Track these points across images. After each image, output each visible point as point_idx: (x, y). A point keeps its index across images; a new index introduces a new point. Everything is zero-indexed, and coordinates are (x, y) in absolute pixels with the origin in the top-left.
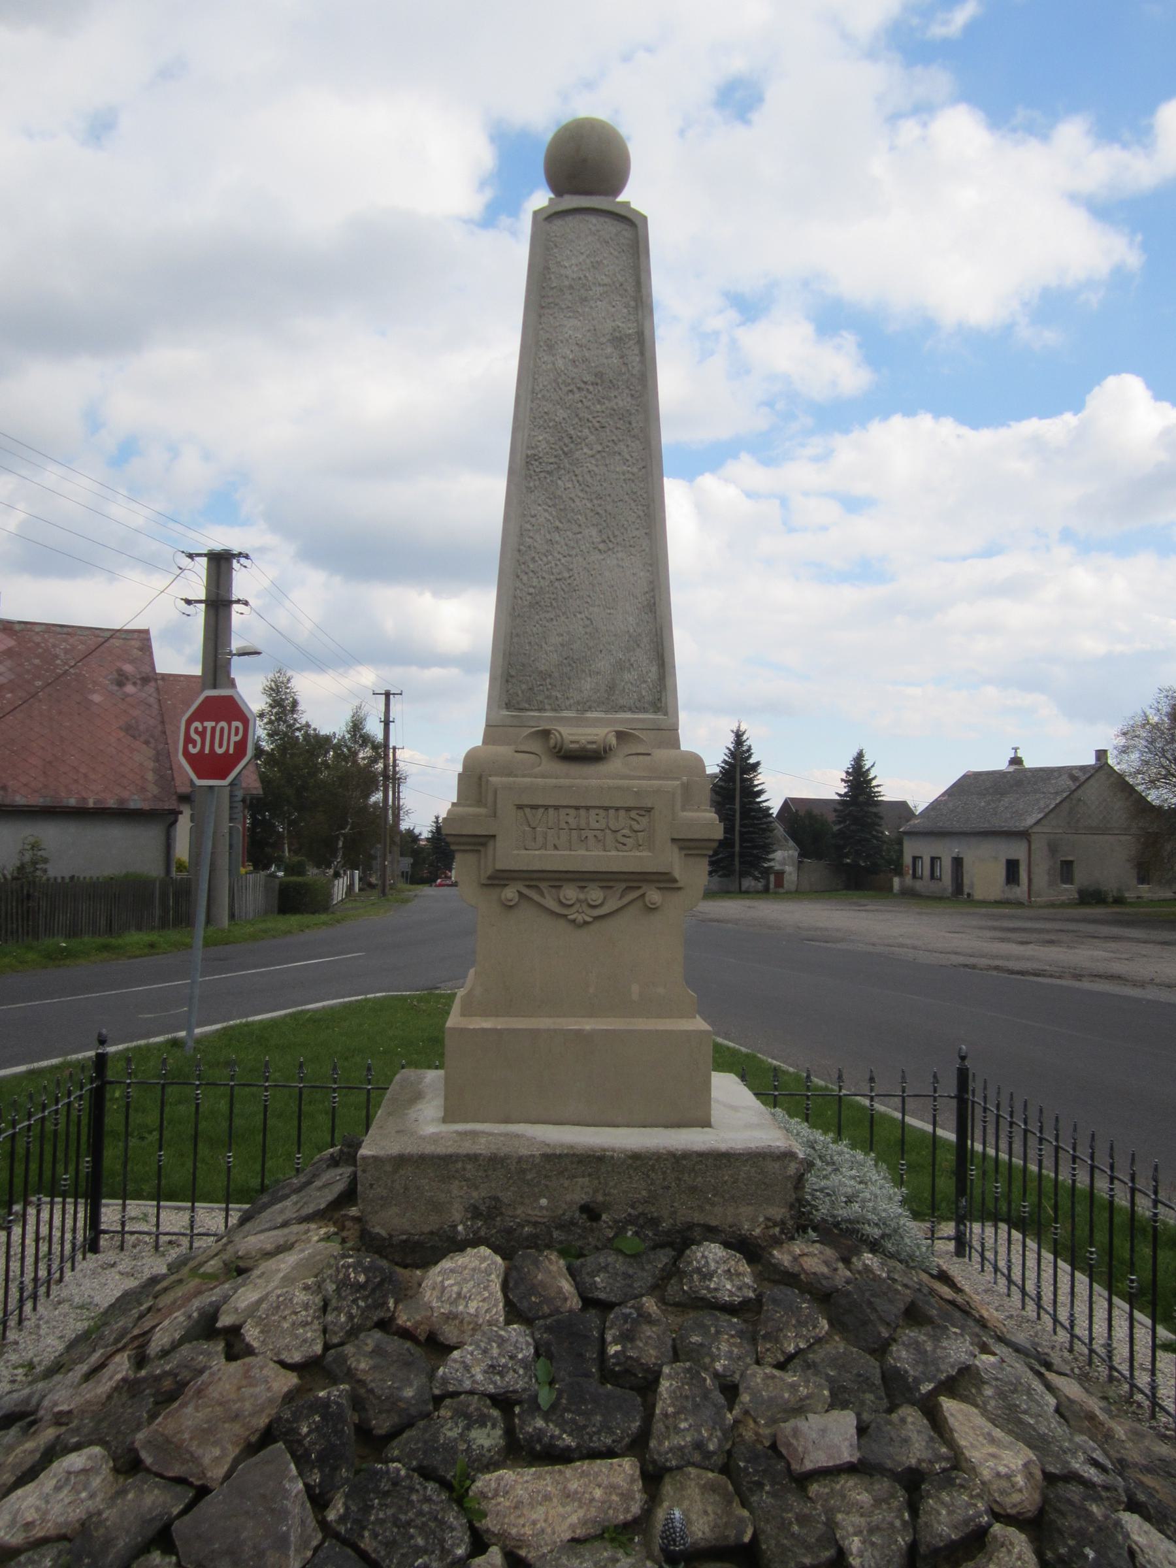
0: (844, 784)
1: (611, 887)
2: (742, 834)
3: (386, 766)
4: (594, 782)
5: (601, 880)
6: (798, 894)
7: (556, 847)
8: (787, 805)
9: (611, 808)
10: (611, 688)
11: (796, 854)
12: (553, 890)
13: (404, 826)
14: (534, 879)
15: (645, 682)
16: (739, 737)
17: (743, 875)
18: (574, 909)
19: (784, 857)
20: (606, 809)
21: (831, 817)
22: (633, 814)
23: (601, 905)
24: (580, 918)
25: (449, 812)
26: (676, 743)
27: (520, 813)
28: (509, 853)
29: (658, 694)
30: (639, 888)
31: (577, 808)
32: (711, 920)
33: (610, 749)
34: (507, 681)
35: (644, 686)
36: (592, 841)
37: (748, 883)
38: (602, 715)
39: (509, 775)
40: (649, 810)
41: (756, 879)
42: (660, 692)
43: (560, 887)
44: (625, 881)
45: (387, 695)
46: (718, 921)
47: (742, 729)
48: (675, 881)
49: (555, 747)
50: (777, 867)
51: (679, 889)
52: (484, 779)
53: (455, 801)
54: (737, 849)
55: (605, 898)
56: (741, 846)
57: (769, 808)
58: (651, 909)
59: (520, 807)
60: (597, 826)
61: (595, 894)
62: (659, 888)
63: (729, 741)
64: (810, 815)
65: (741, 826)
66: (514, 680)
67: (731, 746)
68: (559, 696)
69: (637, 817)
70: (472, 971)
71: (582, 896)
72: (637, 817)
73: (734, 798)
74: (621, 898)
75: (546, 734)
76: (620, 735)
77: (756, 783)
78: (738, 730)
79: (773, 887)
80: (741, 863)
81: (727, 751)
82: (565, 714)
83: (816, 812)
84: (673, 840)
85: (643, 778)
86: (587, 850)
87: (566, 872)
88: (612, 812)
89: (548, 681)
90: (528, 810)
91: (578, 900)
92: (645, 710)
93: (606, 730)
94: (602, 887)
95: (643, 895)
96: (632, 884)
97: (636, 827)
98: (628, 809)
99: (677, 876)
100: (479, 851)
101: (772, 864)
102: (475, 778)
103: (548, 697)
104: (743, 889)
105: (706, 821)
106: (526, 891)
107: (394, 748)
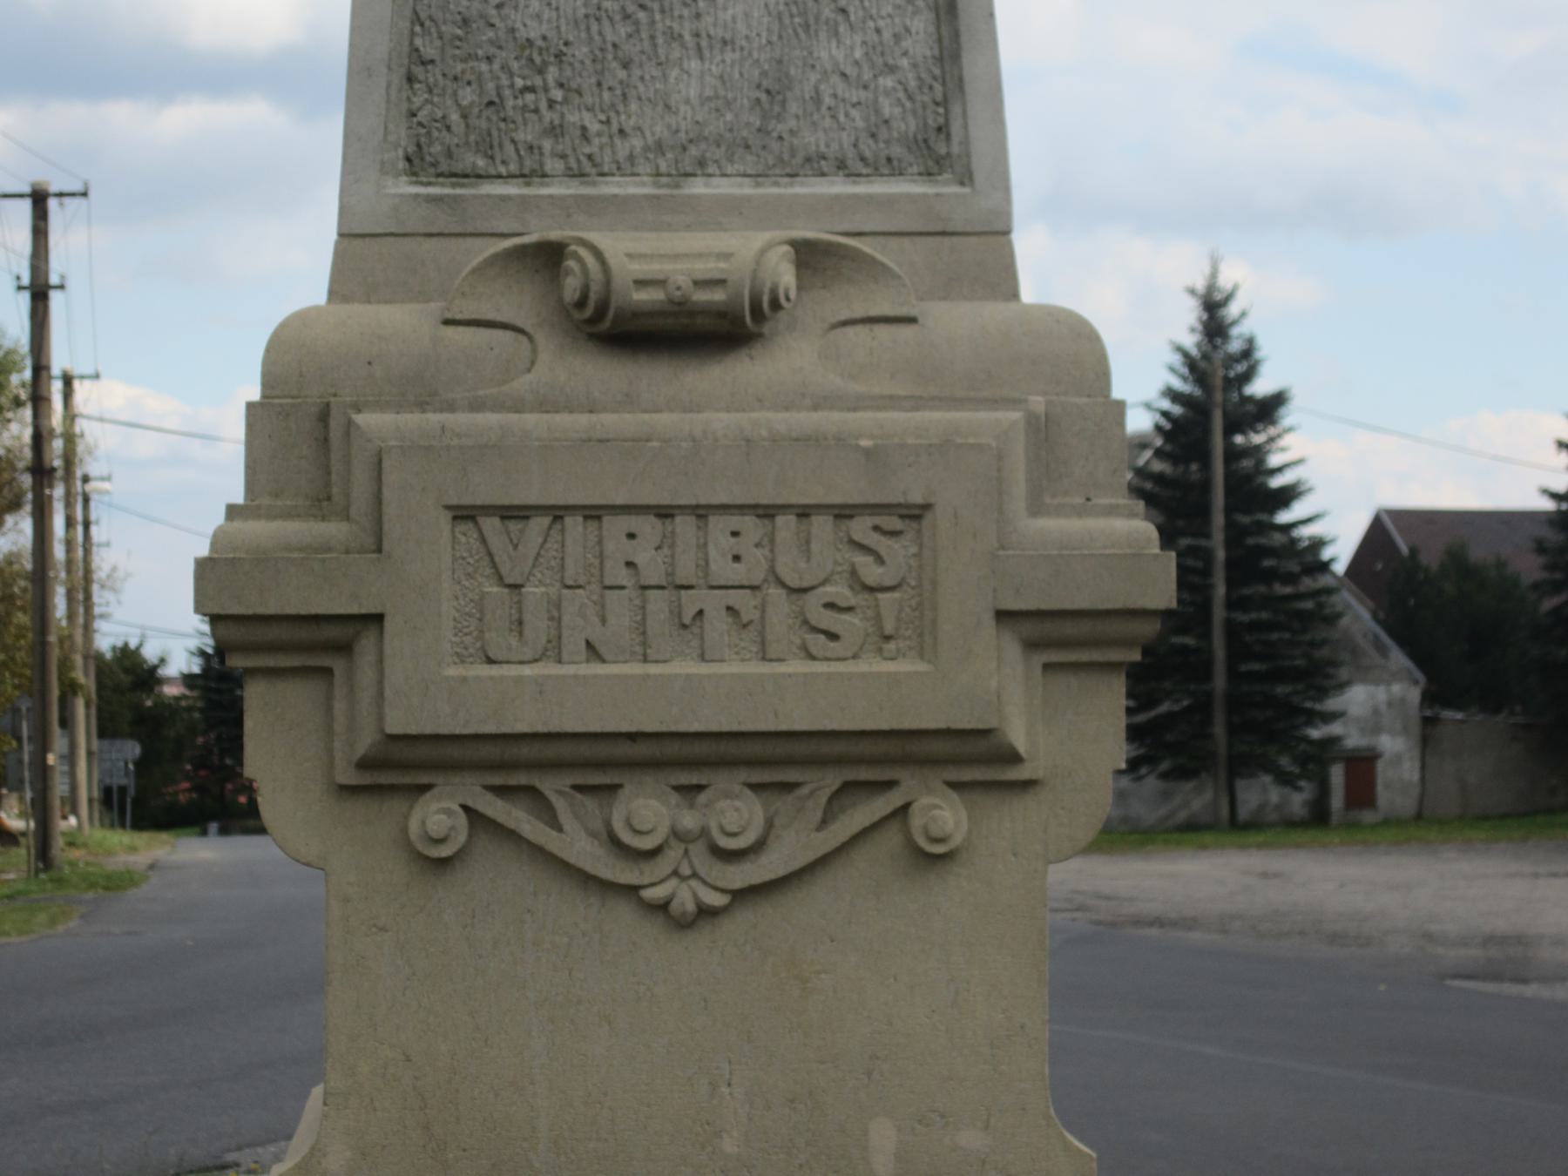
0: (1541, 560)
1: (789, 787)
2: (1232, 629)
3: (39, 440)
4: (721, 421)
5: (750, 763)
6: (1426, 822)
7: (593, 651)
8: (1380, 535)
9: (784, 508)
10: (773, 94)
11: (1414, 695)
12: (589, 803)
13: (109, 655)
14: (517, 763)
15: (892, 69)
16: (1214, 314)
17: (1239, 766)
18: (664, 865)
19: (1373, 706)
20: (767, 512)
21: (1529, 568)
22: (860, 528)
23: (758, 847)
24: (685, 898)
25: (217, 540)
26: (1002, 281)
27: (467, 534)
28: (432, 679)
29: (940, 114)
30: (890, 785)
31: (664, 513)
32: (1138, 922)
33: (776, 305)
34: (410, 79)
35: (888, 82)
36: (717, 624)
37: (1257, 793)
38: (747, 189)
39: (422, 406)
40: (915, 513)
41: (1285, 780)
42: (945, 102)
43: (614, 788)
44: (839, 761)
45: (39, 199)
46: (1159, 922)
47: (1225, 281)
48: (1014, 758)
49: (581, 304)
50: (1354, 741)
51: (1028, 785)
52: (336, 424)
53: (239, 498)
54: (1220, 682)
55: (769, 825)
56: (1232, 673)
57: (1318, 544)
58: (931, 860)
59: (464, 515)
60: (736, 573)
61: (735, 811)
62: (955, 786)
63: (1184, 326)
64: (1457, 561)
65: (1231, 605)
66: (434, 75)
67: (1190, 341)
68: (594, 127)
69: (873, 540)
70: (317, 1092)
71: (689, 821)
72: (873, 540)
73: (1204, 511)
74: (824, 823)
75: (550, 256)
76: (809, 256)
77: (1274, 460)
78: (1211, 287)
79: (1340, 799)
80: (1232, 730)
81: (1177, 360)
82: (611, 187)
83: (1478, 553)
84: (1003, 616)
85: (892, 402)
86: (703, 658)
87: (633, 737)
88: (786, 522)
89: (552, 73)
90: (490, 525)
91: (676, 834)
92: (893, 168)
93: (760, 239)
94: (756, 788)
95: (904, 809)
96: (865, 774)
97: (872, 573)
98: (843, 513)
99: (1021, 743)
100: (328, 672)
101: (1335, 729)
102: (305, 424)
103: (555, 131)
104: (1243, 813)
105: (1117, 551)
106: (494, 808)
107: (68, 380)
